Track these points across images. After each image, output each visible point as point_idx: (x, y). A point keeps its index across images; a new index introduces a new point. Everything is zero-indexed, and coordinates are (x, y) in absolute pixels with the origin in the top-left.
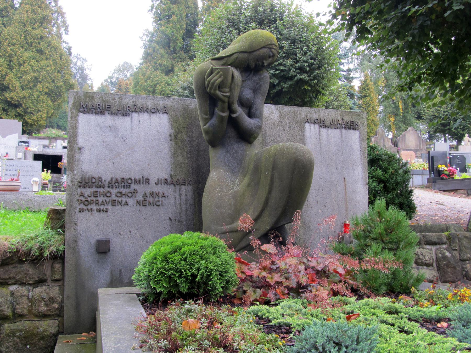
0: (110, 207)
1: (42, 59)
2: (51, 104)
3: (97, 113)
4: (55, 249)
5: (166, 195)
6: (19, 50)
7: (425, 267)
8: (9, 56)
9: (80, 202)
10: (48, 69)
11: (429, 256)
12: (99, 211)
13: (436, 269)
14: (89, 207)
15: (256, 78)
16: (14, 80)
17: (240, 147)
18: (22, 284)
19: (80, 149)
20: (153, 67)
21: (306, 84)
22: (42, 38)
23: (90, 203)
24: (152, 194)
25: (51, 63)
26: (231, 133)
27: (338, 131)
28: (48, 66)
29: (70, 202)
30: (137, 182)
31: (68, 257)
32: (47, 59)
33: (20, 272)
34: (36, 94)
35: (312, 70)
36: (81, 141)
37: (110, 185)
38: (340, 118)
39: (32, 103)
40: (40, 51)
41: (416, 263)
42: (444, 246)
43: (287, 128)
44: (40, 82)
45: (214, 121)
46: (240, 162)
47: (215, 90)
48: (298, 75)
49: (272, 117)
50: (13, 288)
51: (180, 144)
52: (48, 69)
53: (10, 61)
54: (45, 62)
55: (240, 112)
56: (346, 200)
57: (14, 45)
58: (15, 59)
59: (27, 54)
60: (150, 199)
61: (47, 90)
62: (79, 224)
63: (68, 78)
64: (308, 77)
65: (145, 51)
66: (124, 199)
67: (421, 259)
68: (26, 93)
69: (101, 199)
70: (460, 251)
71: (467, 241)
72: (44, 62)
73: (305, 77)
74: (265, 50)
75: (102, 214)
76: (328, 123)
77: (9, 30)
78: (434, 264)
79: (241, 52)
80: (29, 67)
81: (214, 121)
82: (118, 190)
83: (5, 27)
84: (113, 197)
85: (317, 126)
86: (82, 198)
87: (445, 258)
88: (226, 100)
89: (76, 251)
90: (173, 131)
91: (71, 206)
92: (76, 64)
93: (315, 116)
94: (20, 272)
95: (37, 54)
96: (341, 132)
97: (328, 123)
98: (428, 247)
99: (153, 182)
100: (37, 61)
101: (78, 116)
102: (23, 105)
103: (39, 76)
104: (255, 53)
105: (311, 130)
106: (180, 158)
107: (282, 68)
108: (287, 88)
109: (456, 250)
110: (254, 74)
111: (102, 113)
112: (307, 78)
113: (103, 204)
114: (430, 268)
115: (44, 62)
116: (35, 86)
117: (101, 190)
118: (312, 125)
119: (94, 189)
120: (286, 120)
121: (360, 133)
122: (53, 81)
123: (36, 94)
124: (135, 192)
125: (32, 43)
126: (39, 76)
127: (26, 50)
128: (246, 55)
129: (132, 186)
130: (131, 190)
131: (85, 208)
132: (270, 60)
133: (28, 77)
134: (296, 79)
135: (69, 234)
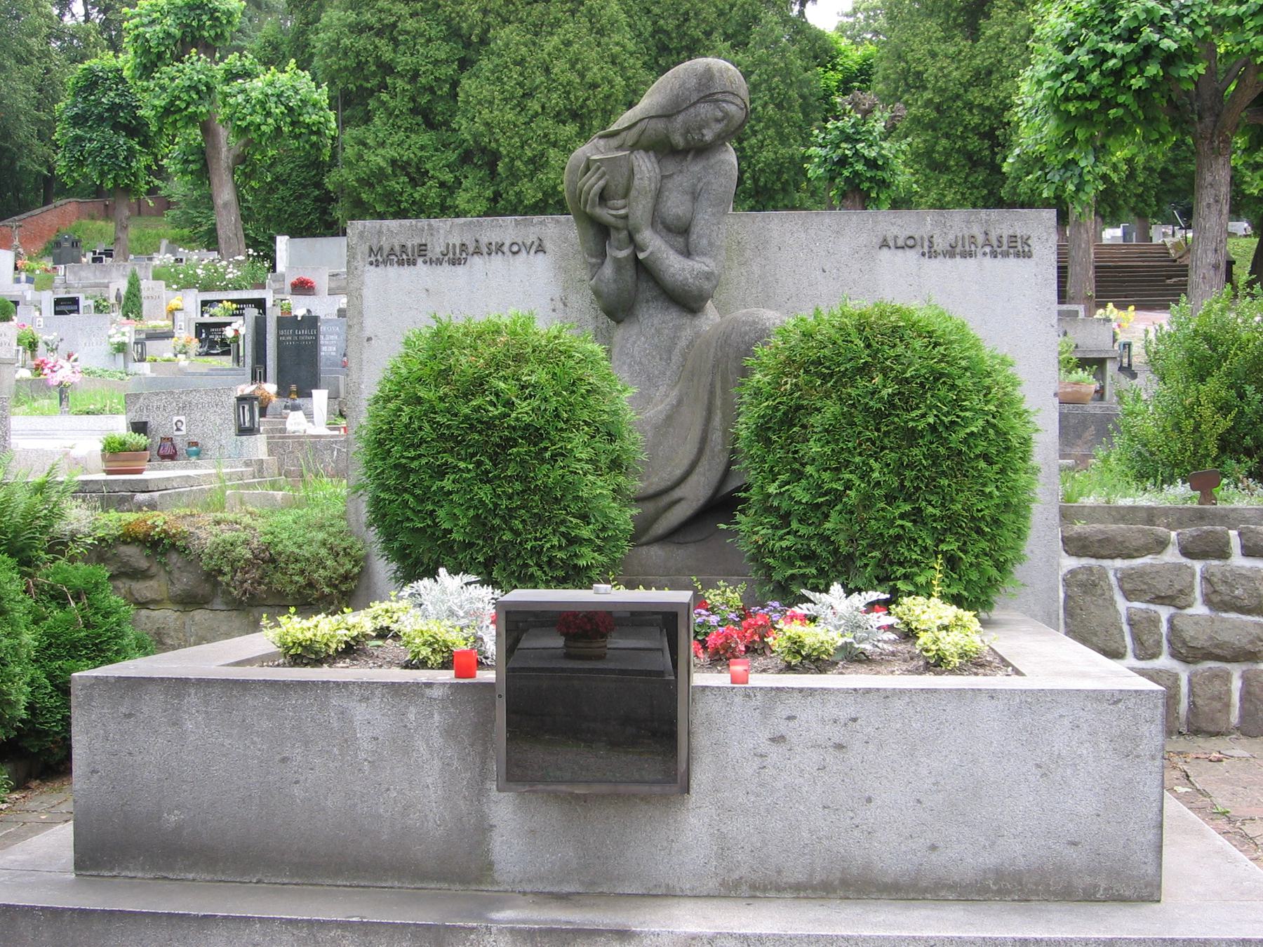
55: (655, 244)
88: (620, 223)
97: (940, 244)
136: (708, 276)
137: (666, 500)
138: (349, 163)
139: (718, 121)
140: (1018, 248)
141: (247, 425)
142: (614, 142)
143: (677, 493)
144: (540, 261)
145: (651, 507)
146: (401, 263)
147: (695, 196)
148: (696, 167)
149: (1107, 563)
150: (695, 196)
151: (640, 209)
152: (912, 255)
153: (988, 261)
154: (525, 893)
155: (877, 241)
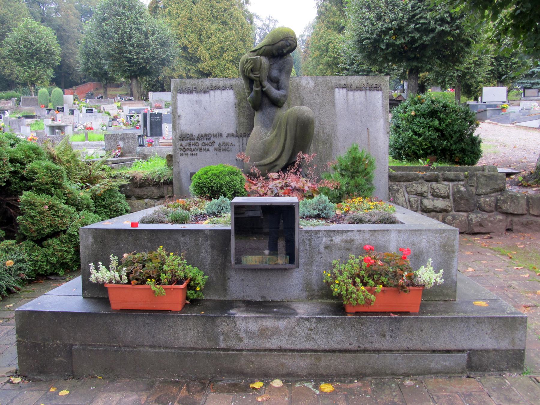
0: (198, 152)
1: (227, 30)
2: (236, 71)
3: (188, 93)
4: (167, 178)
5: (233, 144)
6: (207, 24)
7: (441, 199)
8: (199, 31)
9: (181, 150)
10: (231, 39)
11: (445, 190)
12: (192, 155)
13: (452, 201)
14: (186, 152)
15: (281, 62)
16: (204, 52)
17: (270, 110)
18: (151, 198)
19: (179, 116)
20: (326, 25)
21: (449, 35)
22: (225, 10)
23: (188, 150)
24: (225, 144)
25: (234, 33)
26: (266, 101)
27: (363, 92)
28: (231, 36)
29: (175, 150)
30: (215, 136)
31: (175, 183)
32: (230, 29)
33: (149, 191)
34: (222, 63)
35: (453, 20)
36: (179, 112)
37: (198, 138)
38: (365, 82)
39: (221, 71)
40: (224, 23)
41: (432, 195)
42: (462, 183)
43: (320, 93)
44: (226, 51)
45: (253, 94)
46: (272, 120)
47: (249, 74)
48: (438, 27)
49: (308, 86)
50: (146, 200)
51: (242, 109)
52: (231, 39)
53: (200, 35)
54: (229, 32)
55: (268, 86)
56: (369, 145)
57: (202, 20)
58: (204, 33)
59: (214, 27)
60: (223, 147)
61: (231, 58)
62: (180, 163)
63: (249, 45)
64: (450, 27)
65: (318, 11)
66: (207, 147)
67: (436, 192)
68: (215, 63)
69: (193, 147)
70: (477, 187)
71: (485, 179)
72: (228, 33)
73: (447, 28)
74: (283, 42)
75: (194, 157)
76: (354, 87)
77: (198, 7)
78: (451, 197)
79: (267, 45)
80: (216, 39)
81: (253, 94)
82: (203, 142)
83: (194, 4)
84: (200, 146)
85: (345, 90)
86: (182, 147)
87: (459, 192)
88: (258, 79)
89: (179, 180)
90: (237, 101)
91: (175, 152)
92: (269, 27)
93: (343, 82)
94: (149, 191)
95: (222, 26)
96: (366, 93)
97: (354, 87)
98: (446, 183)
99: (225, 135)
100: (222, 32)
101: (177, 95)
102: (213, 74)
103: (224, 46)
104: (277, 45)
105: (340, 94)
106: (242, 119)
107: (422, 21)
108: (429, 41)
109: (473, 186)
110: (280, 59)
111: (191, 92)
112: (448, 29)
113: (194, 150)
114: (445, 200)
115: (228, 33)
116: (221, 55)
117: (193, 142)
118: (341, 90)
119: (188, 141)
120: (320, 87)
121: (383, 93)
122: (237, 49)
123: (222, 63)
124: (214, 142)
125: (217, 16)
126: (224, 46)
127: (212, 23)
128: (270, 47)
129: (212, 138)
130: (211, 141)
131: (184, 153)
132: (289, 48)
133: (215, 48)
134: (437, 31)
135: (175, 169)
138: (196, 292)
141: (142, 144)
142: (256, 53)
143: (275, 164)
151: (264, 75)
154: (160, 347)
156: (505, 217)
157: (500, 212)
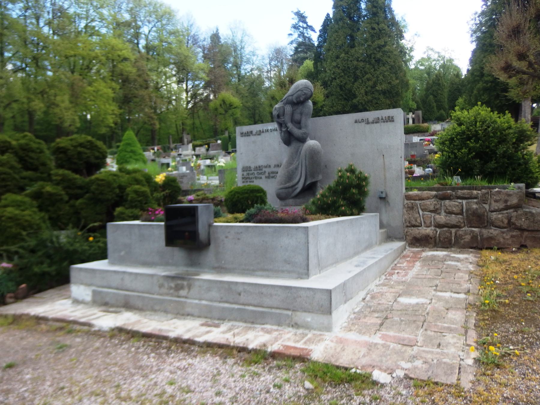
24: (273, 173)
30: (266, 167)
41: (445, 212)
66: (260, 176)
74: (299, 92)
97: (371, 120)
99: (272, 166)
130: (263, 171)
136: (305, 133)
137: (294, 188)
139: (303, 95)
140: (391, 119)
143: (296, 186)
144: (275, 133)
145: (290, 190)
146: (247, 136)
147: (301, 114)
148: (301, 107)
149: (417, 202)
150: (301, 114)
152: (363, 124)
153: (383, 124)
155: (354, 122)
156: (519, 233)
157: (513, 228)
